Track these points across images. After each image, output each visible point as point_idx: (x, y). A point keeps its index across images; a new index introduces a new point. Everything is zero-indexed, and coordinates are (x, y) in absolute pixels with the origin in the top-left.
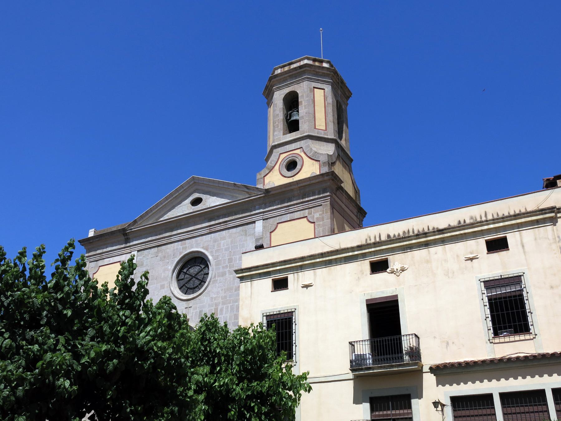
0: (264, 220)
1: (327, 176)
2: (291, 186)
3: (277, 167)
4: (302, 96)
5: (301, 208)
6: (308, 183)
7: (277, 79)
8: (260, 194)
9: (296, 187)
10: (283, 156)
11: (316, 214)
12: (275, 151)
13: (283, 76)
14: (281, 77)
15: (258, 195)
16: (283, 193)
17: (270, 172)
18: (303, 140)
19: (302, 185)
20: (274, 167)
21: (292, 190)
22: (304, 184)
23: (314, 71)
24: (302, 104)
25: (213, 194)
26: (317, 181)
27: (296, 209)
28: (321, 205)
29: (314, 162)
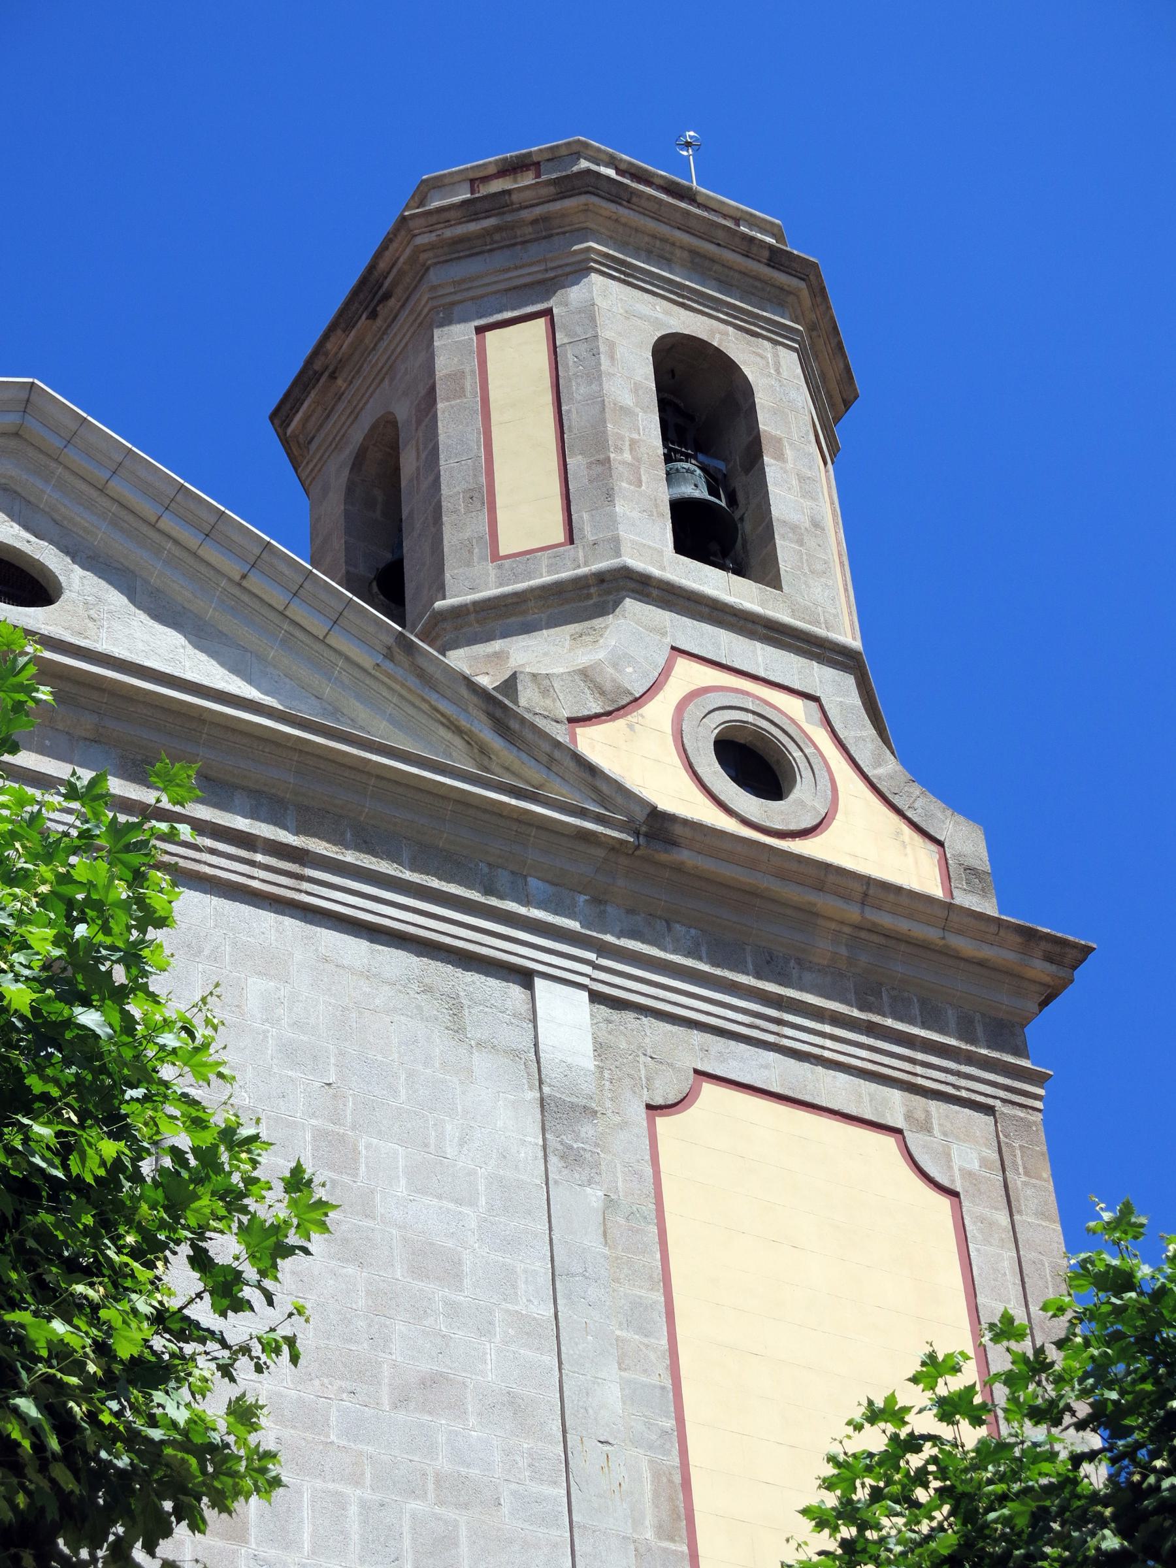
0: (596, 997)
1: (1049, 958)
2: (820, 887)
3: (659, 712)
5: (860, 1058)
6: (931, 934)
7: (623, 212)
8: (599, 819)
9: (853, 913)
11: (963, 1144)
12: (849, 681)
13: (664, 230)
14: (651, 225)
15: (582, 813)
16: (747, 899)
18: (821, 659)
19: (885, 920)
20: (636, 701)
21: (808, 917)
22: (904, 926)
24: (780, 457)
25: (164, 611)
26: (986, 952)
27: (831, 1050)
28: (989, 1110)
29: (906, 830)
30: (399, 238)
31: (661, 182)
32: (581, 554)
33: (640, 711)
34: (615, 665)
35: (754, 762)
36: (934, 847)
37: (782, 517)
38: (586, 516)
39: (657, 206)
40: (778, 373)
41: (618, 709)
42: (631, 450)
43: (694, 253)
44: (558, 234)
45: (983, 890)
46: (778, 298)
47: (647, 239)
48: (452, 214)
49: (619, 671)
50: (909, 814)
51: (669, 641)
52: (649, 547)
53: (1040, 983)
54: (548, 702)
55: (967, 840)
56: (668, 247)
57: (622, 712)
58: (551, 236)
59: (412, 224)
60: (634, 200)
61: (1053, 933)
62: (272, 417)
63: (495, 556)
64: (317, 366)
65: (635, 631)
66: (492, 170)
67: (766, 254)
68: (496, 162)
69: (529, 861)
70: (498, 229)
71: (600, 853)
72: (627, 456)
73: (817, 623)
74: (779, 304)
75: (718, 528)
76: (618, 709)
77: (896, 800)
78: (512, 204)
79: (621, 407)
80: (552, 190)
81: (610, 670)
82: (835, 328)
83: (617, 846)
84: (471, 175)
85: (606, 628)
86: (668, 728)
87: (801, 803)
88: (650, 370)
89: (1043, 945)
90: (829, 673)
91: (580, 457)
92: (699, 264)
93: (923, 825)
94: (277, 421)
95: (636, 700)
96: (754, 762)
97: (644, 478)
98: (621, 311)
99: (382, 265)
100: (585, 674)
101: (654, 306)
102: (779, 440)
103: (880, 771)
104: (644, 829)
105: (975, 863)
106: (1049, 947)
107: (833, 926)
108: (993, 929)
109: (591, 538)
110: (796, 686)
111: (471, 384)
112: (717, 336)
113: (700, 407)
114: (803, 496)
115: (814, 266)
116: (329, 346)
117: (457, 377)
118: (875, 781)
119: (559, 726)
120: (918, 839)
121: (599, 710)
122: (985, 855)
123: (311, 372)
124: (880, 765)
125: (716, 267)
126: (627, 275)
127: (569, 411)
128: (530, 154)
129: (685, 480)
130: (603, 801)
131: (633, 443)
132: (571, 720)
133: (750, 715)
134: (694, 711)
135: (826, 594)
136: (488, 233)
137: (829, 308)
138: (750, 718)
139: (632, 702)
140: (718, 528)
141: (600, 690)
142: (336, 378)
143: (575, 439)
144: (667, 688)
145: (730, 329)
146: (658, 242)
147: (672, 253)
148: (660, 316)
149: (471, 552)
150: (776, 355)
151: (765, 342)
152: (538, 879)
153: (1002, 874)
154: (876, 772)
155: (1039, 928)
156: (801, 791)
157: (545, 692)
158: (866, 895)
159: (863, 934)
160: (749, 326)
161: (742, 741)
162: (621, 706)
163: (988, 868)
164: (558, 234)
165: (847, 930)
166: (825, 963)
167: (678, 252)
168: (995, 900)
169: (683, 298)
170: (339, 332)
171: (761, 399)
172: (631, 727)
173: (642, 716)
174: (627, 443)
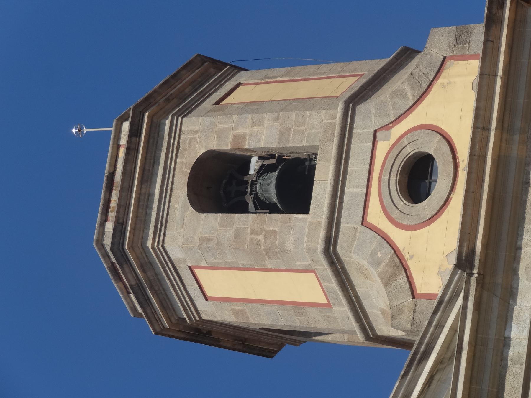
3: (399, 237)
4: (220, 135)
8: (466, 299)
10: (376, 215)
17: (406, 270)
20: (396, 252)
23: (168, 100)
24: (243, 137)
30: (166, 333)
31: (108, 194)
32: (320, 267)
33: (401, 250)
34: (378, 264)
35: (416, 177)
36: (448, 63)
37: (277, 140)
38: (298, 263)
39: (122, 208)
40: (196, 132)
41: (402, 264)
42: (257, 235)
43: (142, 181)
44: (148, 259)
45: (468, 32)
46: (155, 129)
47: (140, 210)
48: (149, 311)
49: (381, 262)
50: (431, 78)
51: (359, 226)
52: (309, 230)
53: (517, 8)
54: (406, 310)
55: (439, 41)
56: (142, 197)
57: (403, 262)
58: (150, 262)
59: (158, 330)
60: (121, 221)
61: (487, 5)
62: (272, 357)
63: (328, 306)
64: (240, 347)
65: (355, 254)
66: (121, 284)
67: (134, 139)
68: (117, 283)
69: (497, 337)
70: (152, 288)
71: (485, 294)
72: (261, 237)
73: (333, 125)
74: (159, 126)
75: (292, 182)
76: (402, 264)
77: (425, 86)
78: (137, 283)
79: (235, 237)
80: (125, 266)
81: (382, 267)
82: (164, 83)
83: (480, 285)
84: (126, 294)
85: (358, 263)
86: (408, 233)
87: (436, 150)
88: (211, 216)
89: (494, 11)
90: (358, 121)
91: (266, 262)
92: (147, 178)
93: (436, 69)
94: (273, 355)
95: (395, 252)
96: (416, 177)
97: (271, 228)
98: (182, 230)
99: (182, 336)
100: (386, 284)
101: (176, 209)
102: (235, 137)
103: (410, 94)
104: (468, 271)
105: (453, 35)
106: (495, 7)
107: (504, 145)
108: (490, 44)
109: (309, 262)
110: (371, 145)
111: (237, 307)
112: (184, 169)
113: (222, 184)
114: (263, 125)
115: (135, 108)
116: (229, 345)
117: (235, 313)
118: (416, 99)
119: (418, 305)
120: (445, 73)
121: (405, 278)
122: (445, 30)
123: (244, 349)
124: (406, 94)
125: (147, 168)
126: (161, 226)
127: (243, 265)
128: (109, 268)
129: (267, 190)
130: (451, 358)
131: (253, 232)
132: (413, 297)
133: (391, 178)
134: (395, 214)
135: (315, 117)
136: (155, 293)
137: (155, 91)
138: (393, 178)
139: (397, 255)
140: (292, 182)
141: (394, 275)
142: (245, 338)
143: (264, 257)
144: (385, 231)
145: (178, 160)
146: (141, 203)
147: (145, 194)
148: (180, 205)
149: (329, 317)
150: (189, 132)
151: (181, 138)
152: (505, 329)
153: (460, 20)
154: (410, 94)
155: (485, 15)
156: (432, 146)
157: (401, 311)
158: (483, 129)
159: (506, 125)
160: (175, 149)
161: (407, 179)
162: (400, 263)
163: (454, 28)
164: (148, 259)
165: (505, 136)
166: (525, 147)
167: (143, 191)
168: (472, 25)
169: (167, 189)
170: (221, 343)
171: (214, 145)
172: (411, 257)
173: (404, 249)
174: (254, 236)
